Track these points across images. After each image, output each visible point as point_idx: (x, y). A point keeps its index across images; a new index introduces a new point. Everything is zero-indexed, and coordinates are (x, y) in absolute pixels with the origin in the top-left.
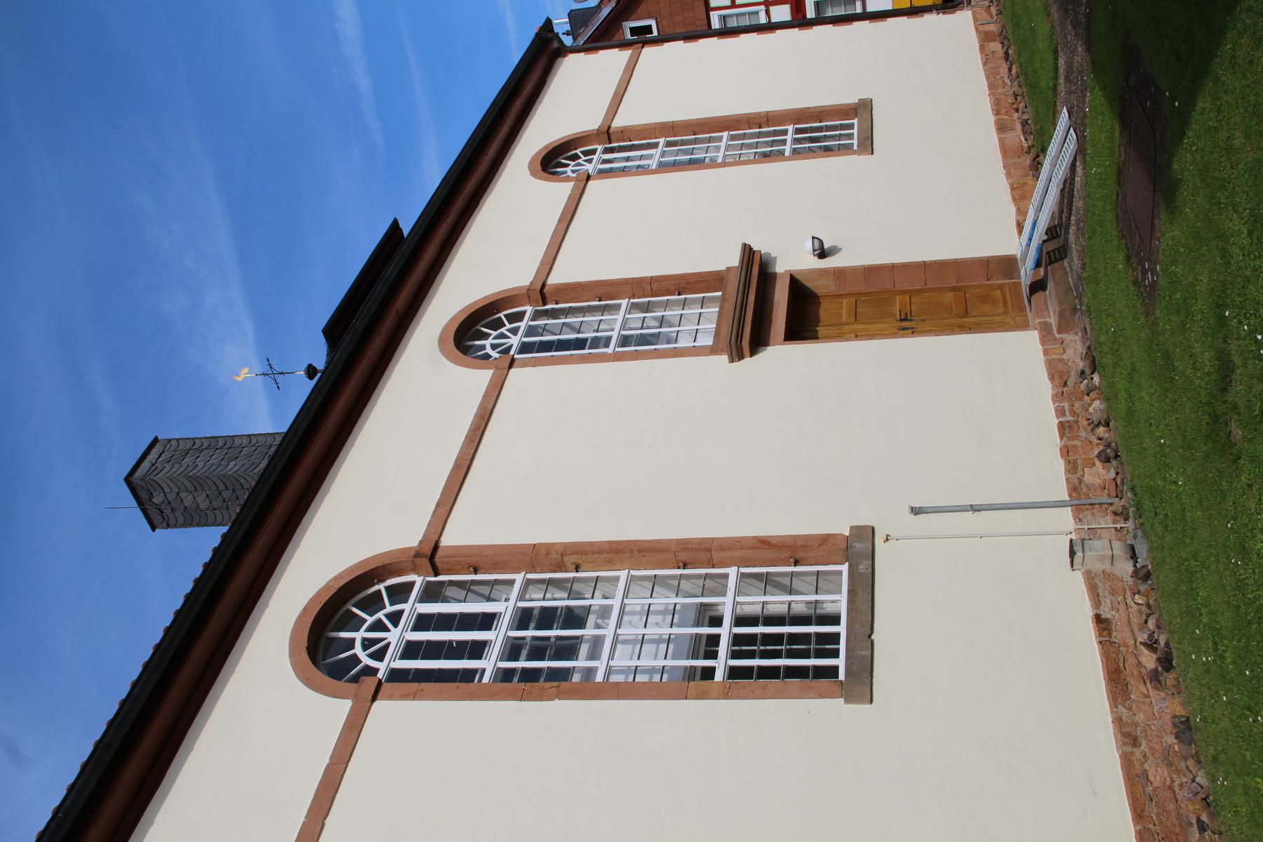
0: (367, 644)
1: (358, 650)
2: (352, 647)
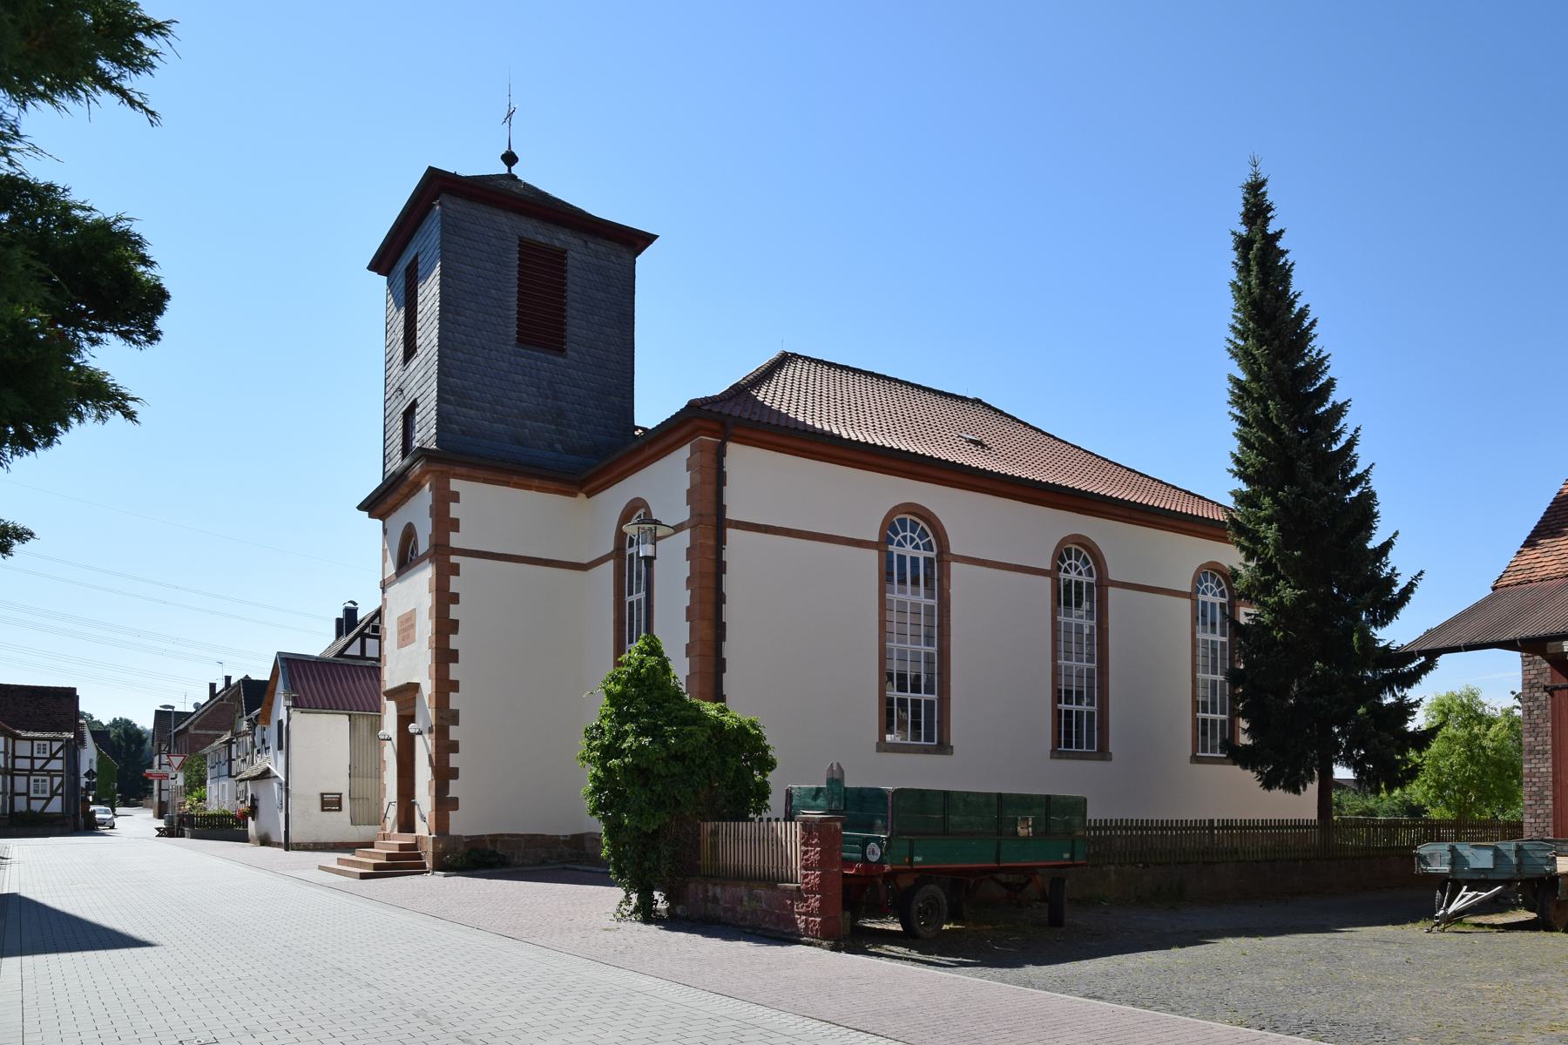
0: (1070, 565)
1: (1068, 562)
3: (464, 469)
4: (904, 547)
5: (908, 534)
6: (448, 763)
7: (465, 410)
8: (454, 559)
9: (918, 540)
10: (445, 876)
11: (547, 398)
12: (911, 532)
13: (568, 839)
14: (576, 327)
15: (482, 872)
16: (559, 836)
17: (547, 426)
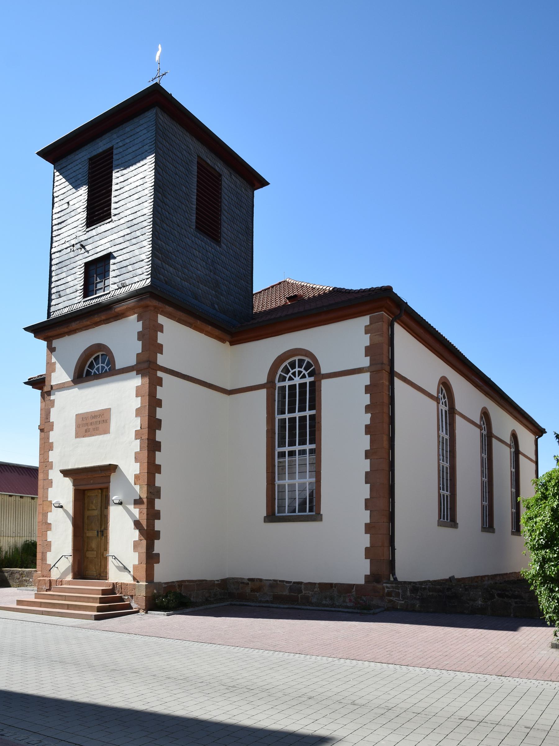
3: (171, 308)
4: (293, 379)
6: (154, 527)
7: (167, 266)
8: (160, 374)
9: (290, 374)
10: (168, 615)
11: (211, 272)
13: (219, 582)
14: (226, 229)
15: (188, 610)
16: (214, 581)
17: (211, 290)
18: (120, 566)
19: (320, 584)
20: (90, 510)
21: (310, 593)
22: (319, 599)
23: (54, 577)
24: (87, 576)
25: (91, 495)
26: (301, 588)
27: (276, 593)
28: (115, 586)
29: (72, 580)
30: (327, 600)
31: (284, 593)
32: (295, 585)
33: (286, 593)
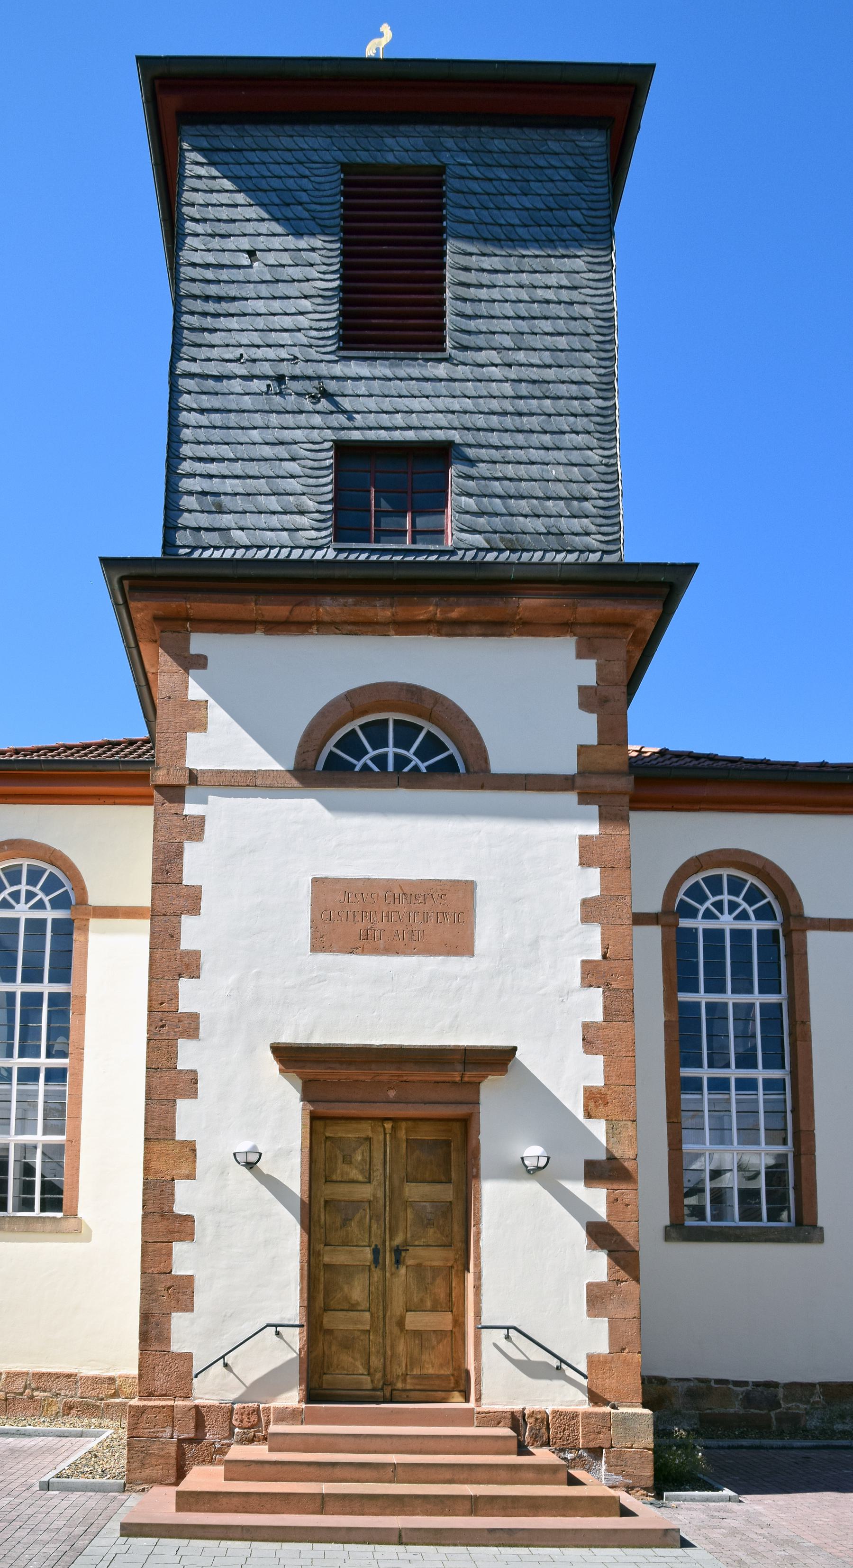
1: (713, 899)
2: (714, 895)
4: (717, 918)
5: (726, 897)
12: (730, 893)
18: (533, 1358)
19: (823, 1385)
20: (337, 1182)
21: (802, 1406)
22: (826, 1420)
23: (207, 1397)
24: (327, 1392)
25: (340, 1135)
26: (776, 1396)
27: (708, 1411)
28: (521, 1422)
29: (303, 1405)
30: (847, 1421)
31: (732, 1411)
32: (760, 1389)
33: (736, 1408)
